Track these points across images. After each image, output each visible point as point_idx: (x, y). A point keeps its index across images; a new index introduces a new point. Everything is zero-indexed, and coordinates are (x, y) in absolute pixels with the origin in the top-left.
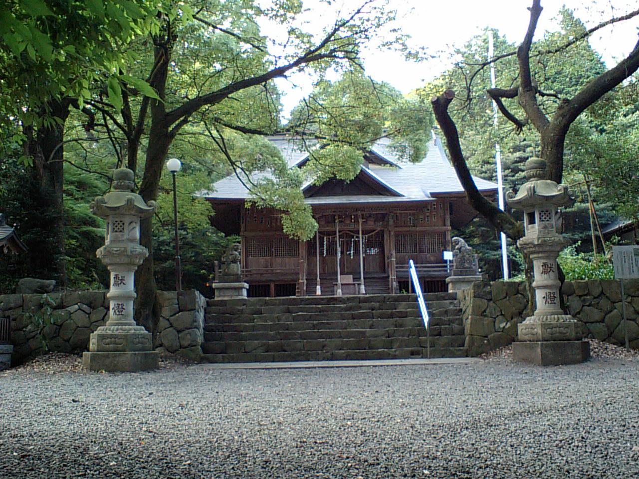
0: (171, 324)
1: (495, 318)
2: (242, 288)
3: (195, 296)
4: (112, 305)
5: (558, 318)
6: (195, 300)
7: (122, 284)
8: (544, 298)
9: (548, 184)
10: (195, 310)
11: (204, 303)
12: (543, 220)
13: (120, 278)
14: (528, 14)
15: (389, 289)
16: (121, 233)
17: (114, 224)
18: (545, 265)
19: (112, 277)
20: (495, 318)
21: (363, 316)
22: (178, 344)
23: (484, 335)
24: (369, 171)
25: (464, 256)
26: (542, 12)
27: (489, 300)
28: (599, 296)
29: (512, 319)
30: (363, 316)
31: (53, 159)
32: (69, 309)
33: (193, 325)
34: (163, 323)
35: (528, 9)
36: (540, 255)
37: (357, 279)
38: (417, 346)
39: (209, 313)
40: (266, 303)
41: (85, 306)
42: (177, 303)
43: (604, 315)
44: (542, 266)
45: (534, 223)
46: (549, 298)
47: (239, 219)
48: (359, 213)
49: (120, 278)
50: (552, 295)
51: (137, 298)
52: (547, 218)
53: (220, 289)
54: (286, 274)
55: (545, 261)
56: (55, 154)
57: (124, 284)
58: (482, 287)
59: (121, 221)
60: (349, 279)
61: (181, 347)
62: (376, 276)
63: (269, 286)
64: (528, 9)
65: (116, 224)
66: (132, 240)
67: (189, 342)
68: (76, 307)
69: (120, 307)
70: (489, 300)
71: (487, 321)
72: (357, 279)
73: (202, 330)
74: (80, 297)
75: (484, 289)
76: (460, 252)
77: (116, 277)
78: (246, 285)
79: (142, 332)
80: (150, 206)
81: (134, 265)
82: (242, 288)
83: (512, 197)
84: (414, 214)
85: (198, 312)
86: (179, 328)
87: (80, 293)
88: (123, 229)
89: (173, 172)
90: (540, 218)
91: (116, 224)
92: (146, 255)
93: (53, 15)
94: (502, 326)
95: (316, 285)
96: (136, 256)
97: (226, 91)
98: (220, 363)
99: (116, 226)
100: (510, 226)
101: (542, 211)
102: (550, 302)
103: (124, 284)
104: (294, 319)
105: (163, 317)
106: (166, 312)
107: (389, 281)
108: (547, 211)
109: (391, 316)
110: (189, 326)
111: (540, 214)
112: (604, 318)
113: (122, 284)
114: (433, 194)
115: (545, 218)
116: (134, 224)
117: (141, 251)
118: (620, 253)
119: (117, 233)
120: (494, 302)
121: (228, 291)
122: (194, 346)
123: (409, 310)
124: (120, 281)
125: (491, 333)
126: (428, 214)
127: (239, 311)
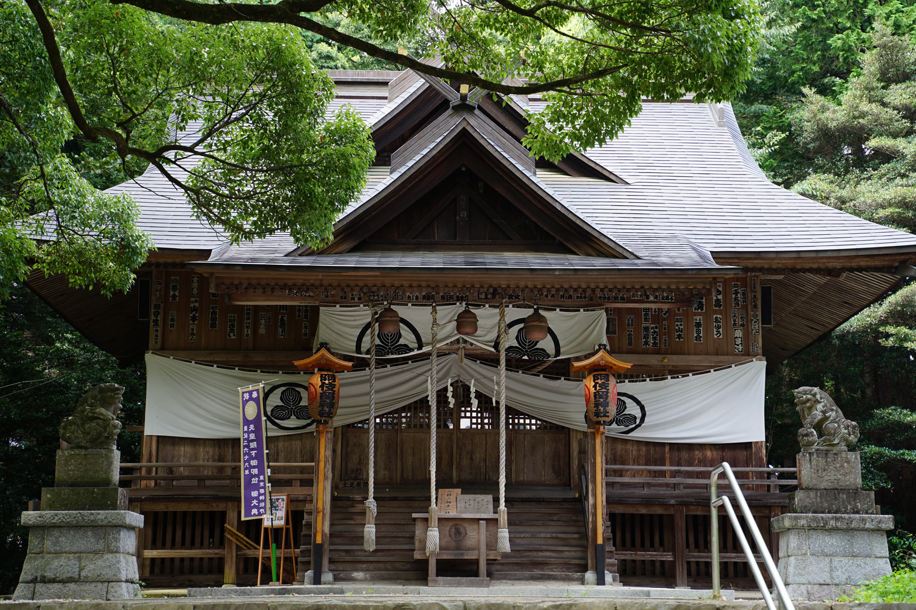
53: (43, 528)
63: (153, 560)
78: (136, 519)
126: (698, 318)
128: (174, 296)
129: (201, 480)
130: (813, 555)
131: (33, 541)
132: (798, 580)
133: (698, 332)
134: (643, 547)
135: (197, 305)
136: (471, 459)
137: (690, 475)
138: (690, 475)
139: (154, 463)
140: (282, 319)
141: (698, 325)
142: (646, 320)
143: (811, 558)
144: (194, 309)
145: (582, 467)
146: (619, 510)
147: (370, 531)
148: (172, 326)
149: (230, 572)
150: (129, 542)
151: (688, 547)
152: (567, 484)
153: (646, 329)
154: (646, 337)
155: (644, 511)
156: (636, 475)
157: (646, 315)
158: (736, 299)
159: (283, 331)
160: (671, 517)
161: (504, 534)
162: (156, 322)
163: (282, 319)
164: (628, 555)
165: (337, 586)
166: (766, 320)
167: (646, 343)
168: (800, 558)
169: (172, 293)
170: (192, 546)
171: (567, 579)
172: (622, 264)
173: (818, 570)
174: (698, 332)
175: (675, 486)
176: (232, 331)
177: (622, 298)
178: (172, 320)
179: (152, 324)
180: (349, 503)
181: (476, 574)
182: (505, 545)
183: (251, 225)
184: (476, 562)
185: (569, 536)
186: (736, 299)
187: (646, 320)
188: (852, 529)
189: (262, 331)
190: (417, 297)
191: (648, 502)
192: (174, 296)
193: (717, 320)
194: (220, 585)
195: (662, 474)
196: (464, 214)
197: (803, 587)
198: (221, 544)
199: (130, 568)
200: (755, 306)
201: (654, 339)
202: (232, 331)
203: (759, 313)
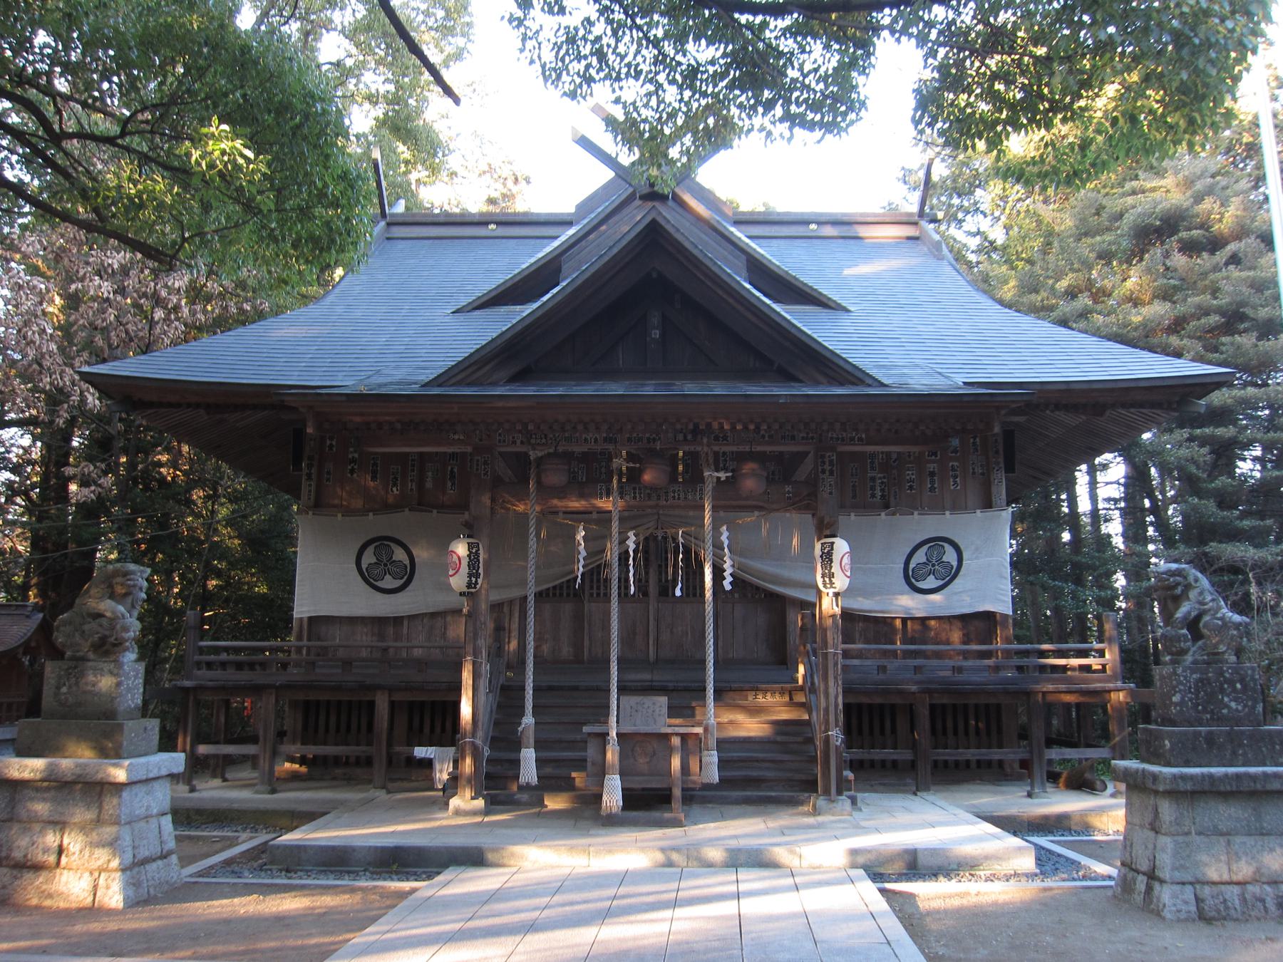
47: (297, 467)
63: (371, 705)
126: (931, 467)
128: (331, 446)
130: (1199, 833)
132: (1178, 876)
133: (932, 482)
135: (356, 455)
136: (672, 632)
139: (305, 642)
140: (452, 471)
141: (932, 474)
142: (872, 468)
143: (1198, 839)
144: (353, 461)
148: (328, 480)
153: (873, 479)
154: (873, 488)
155: (878, 700)
157: (872, 463)
158: (974, 443)
159: (453, 484)
162: (309, 476)
163: (452, 471)
166: (1009, 468)
167: (873, 496)
168: (1180, 839)
169: (328, 442)
174: (932, 482)
176: (395, 484)
177: (860, 439)
178: (328, 473)
179: (304, 478)
180: (652, 544)
185: (791, 739)
186: (974, 443)
187: (872, 468)
189: (429, 485)
190: (596, 440)
192: (331, 446)
193: (953, 469)
196: (656, 334)
197: (1189, 888)
200: (997, 452)
201: (882, 490)
202: (395, 484)
203: (1001, 460)
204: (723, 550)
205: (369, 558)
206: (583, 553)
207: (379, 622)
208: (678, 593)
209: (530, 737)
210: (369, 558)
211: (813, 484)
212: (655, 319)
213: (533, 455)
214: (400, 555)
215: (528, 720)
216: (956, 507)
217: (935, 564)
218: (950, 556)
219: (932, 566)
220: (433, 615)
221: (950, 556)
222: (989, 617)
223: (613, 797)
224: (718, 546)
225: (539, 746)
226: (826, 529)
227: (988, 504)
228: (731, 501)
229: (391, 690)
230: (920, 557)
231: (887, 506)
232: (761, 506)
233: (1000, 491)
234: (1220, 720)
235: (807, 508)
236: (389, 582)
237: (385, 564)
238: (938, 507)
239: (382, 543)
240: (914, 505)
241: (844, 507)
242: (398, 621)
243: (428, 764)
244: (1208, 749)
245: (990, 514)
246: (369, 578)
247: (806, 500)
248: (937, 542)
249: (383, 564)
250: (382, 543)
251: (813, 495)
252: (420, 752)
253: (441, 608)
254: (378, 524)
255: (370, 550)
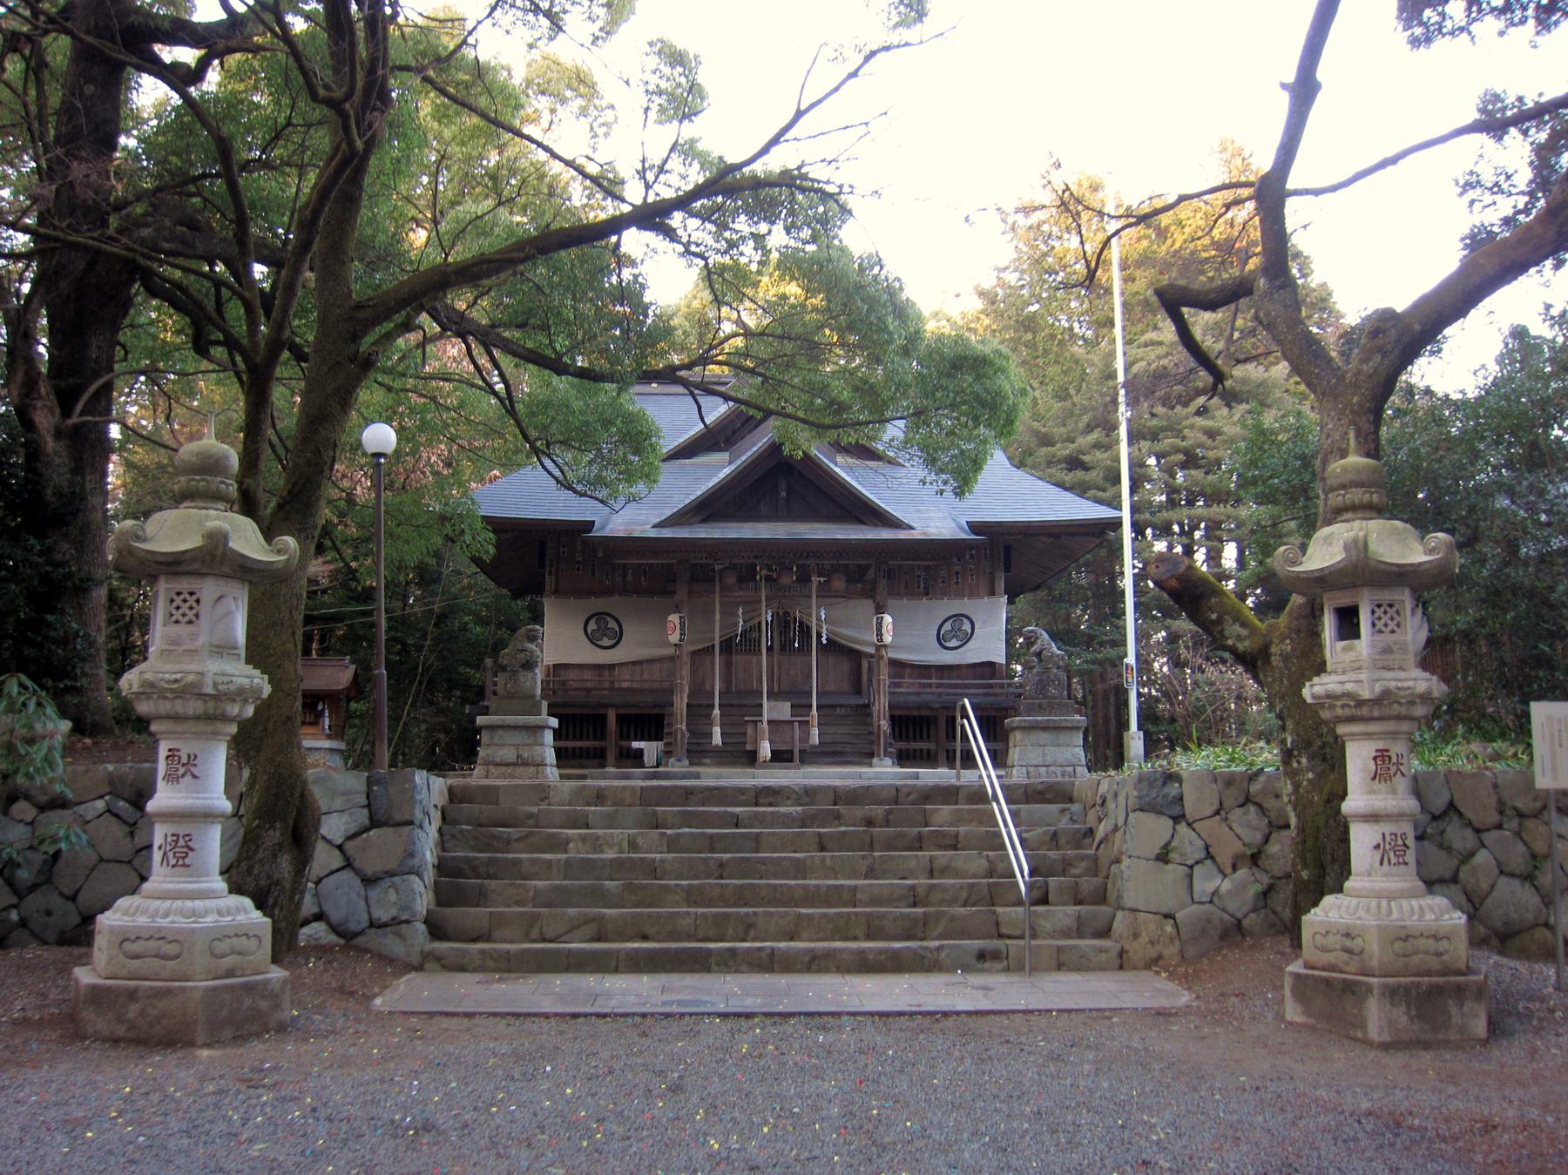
0: (347, 859)
1: (1191, 867)
2: (543, 728)
3: (414, 787)
4: (160, 834)
5: (1421, 908)
6: (412, 797)
7: (188, 778)
8: (1377, 847)
9: (1395, 530)
10: (411, 823)
11: (441, 793)
12: (1380, 632)
13: (184, 760)
14: (1283, 101)
15: (871, 733)
16: (190, 628)
17: (172, 601)
18: (1382, 756)
19: (163, 752)
20: (1191, 867)
21: (843, 842)
22: (365, 916)
23: (1165, 910)
24: (837, 470)
25: (1047, 670)
26: (1319, 95)
27: (1177, 819)
28: (1445, 813)
29: (1234, 868)
30: (843, 842)
31: (81, 415)
32: (81, 809)
33: (408, 866)
34: (323, 858)
35: (1284, 86)
36: (1373, 727)
37: (801, 708)
38: (990, 937)
39: (455, 822)
40: (600, 797)
41: (122, 803)
42: (365, 802)
43: (1456, 862)
44: (1375, 758)
45: (1357, 636)
46: (1388, 851)
47: (542, 565)
48: (811, 562)
49: (184, 760)
50: (1400, 842)
51: (236, 814)
52: (1392, 625)
53: (492, 728)
54: (641, 691)
55: (1380, 745)
56: (86, 404)
57: (194, 776)
58: (1160, 783)
59: (191, 594)
60: (784, 710)
61: (372, 925)
62: (842, 701)
63: (604, 718)
64: (1284, 86)
65: (178, 600)
66: (223, 649)
67: (394, 912)
68: (100, 805)
69: (181, 842)
70: (1177, 819)
71: (1174, 871)
72: (801, 708)
73: (430, 874)
74: (112, 780)
75: (1165, 790)
76: (1040, 660)
77: (172, 754)
78: (554, 722)
79: (241, 918)
80: (279, 552)
81: (230, 720)
82: (543, 728)
83: (1294, 563)
84: (926, 568)
85: (421, 827)
86: (370, 869)
87: (110, 767)
88: (197, 615)
89: (378, 455)
90: (1374, 625)
91: (178, 600)
92: (261, 690)
93: (1287, 993)
94: (1211, 887)
95: (711, 725)
96: (231, 697)
97: (514, 255)
98: (474, 970)
99: (178, 608)
100: (1244, 632)
101: (1379, 606)
102: (1393, 860)
103: (194, 776)
104: (673, 845)
105: (329, 842)
106: (334, 827)
107: (871, 715)
108: (1391, 606)
109: (918, 844)
110: (392, 866)
111: (1373, 612)
112: (1458, 870)
113: (188, 778)
114: (975, 527)
115: (1386, 625)
116: (229, 603)
117: (246, 681)
118: (1549, 718)
119: (177, 628)
120: (1189, 825)
121: (511, 733)
122: (407, 922)
123: (962, 829)
124: (184, 769)
125: (1183, 907)
126: (957, 568)
127: (530, 816)
129: (588, 690)
131: (484, 737)
134: (915, 740)
137: (950, 686)
138: (950, 686)
145: (870, 681)
146: (897, 713)
147: (717, 731)
149: (611, 757)
150: (549, 737)
151: (307, 652)
152: (858, 692)
155: (915, 713)
156: (909, 685)
160: (936, 718)
161: (815, 731)
164: (903, 745)
165: (693, 769)
166: (1007, 569)
170: (581, 739)
171: (860, 764)
172: (902, 535)
173: (1034, 756)
175: (940, 695)
181: (791, 760)
182: (815, 737)
183: (140, 140)
184: (792, 752)
188: (344, 794)
189: (630, 578)
191: (919, 707)
194: (603, 766)
195: (930, 686)
196: (783, 494)
198: (603, 737)
199: (550, 756)
204: (823, 618)
205: (592, 626)
206: (384, 637)
207: (599, 668)
208: (717, 739)
209: (718, 720)
210: (592, 626)
211: (874, 582)
212: (783, 486)
213: (717, 568)
214: (612, 624)
215: (717, 711)
216: (973, 594)
217: (957, 630)
218: (967, 626)
219: (954, 632)
220: (634, 663)
221: (967, 626)
222: (991, 664)
223: (765, 749)
224: (819, 619)
225: (722, 725)
226: (880, 609)
227: (992, 593)
228: (826, 592)
229: (616, 707)
230: (947, 626)
231: (927, 594)
232: (846, 596)
233: (1001, 585)
234: (1045, 697)
235: (871, 597)
236: (606, 642)
237: (603, 631)
238: (960, 595)
239: (600, 616)
240: (945, 594)
241: (893, 593)
242: (611, 667)
243: (640, 752)
244: (1040, 709)
245: (993, 599)
246: (593, 640)
247: (869, 593)
248: (958, 617)
249: (602, 630)
250: (600, 616)
251: (874, 590)
252: (636, 745)
253: (640, 658)
254: (598, 604)
255: (592, 622)
